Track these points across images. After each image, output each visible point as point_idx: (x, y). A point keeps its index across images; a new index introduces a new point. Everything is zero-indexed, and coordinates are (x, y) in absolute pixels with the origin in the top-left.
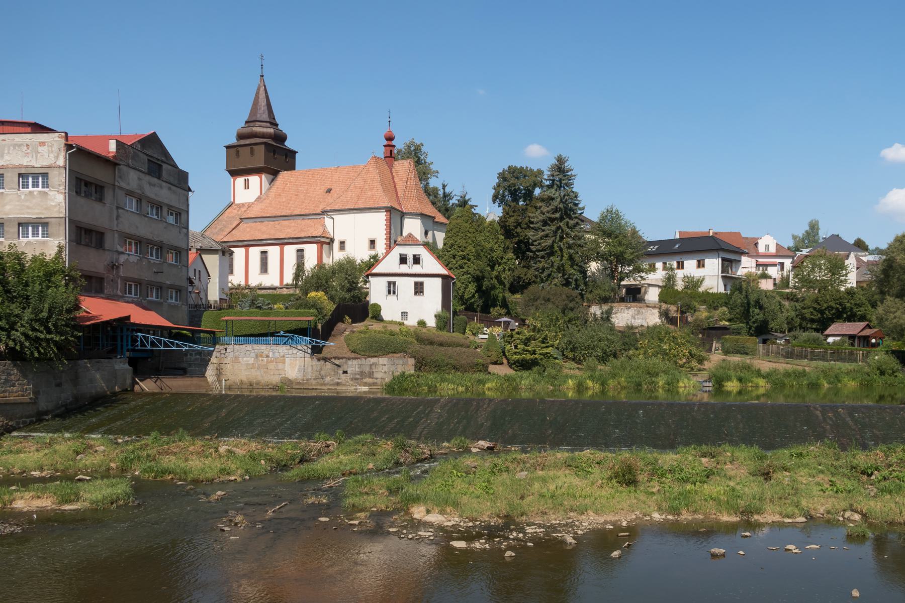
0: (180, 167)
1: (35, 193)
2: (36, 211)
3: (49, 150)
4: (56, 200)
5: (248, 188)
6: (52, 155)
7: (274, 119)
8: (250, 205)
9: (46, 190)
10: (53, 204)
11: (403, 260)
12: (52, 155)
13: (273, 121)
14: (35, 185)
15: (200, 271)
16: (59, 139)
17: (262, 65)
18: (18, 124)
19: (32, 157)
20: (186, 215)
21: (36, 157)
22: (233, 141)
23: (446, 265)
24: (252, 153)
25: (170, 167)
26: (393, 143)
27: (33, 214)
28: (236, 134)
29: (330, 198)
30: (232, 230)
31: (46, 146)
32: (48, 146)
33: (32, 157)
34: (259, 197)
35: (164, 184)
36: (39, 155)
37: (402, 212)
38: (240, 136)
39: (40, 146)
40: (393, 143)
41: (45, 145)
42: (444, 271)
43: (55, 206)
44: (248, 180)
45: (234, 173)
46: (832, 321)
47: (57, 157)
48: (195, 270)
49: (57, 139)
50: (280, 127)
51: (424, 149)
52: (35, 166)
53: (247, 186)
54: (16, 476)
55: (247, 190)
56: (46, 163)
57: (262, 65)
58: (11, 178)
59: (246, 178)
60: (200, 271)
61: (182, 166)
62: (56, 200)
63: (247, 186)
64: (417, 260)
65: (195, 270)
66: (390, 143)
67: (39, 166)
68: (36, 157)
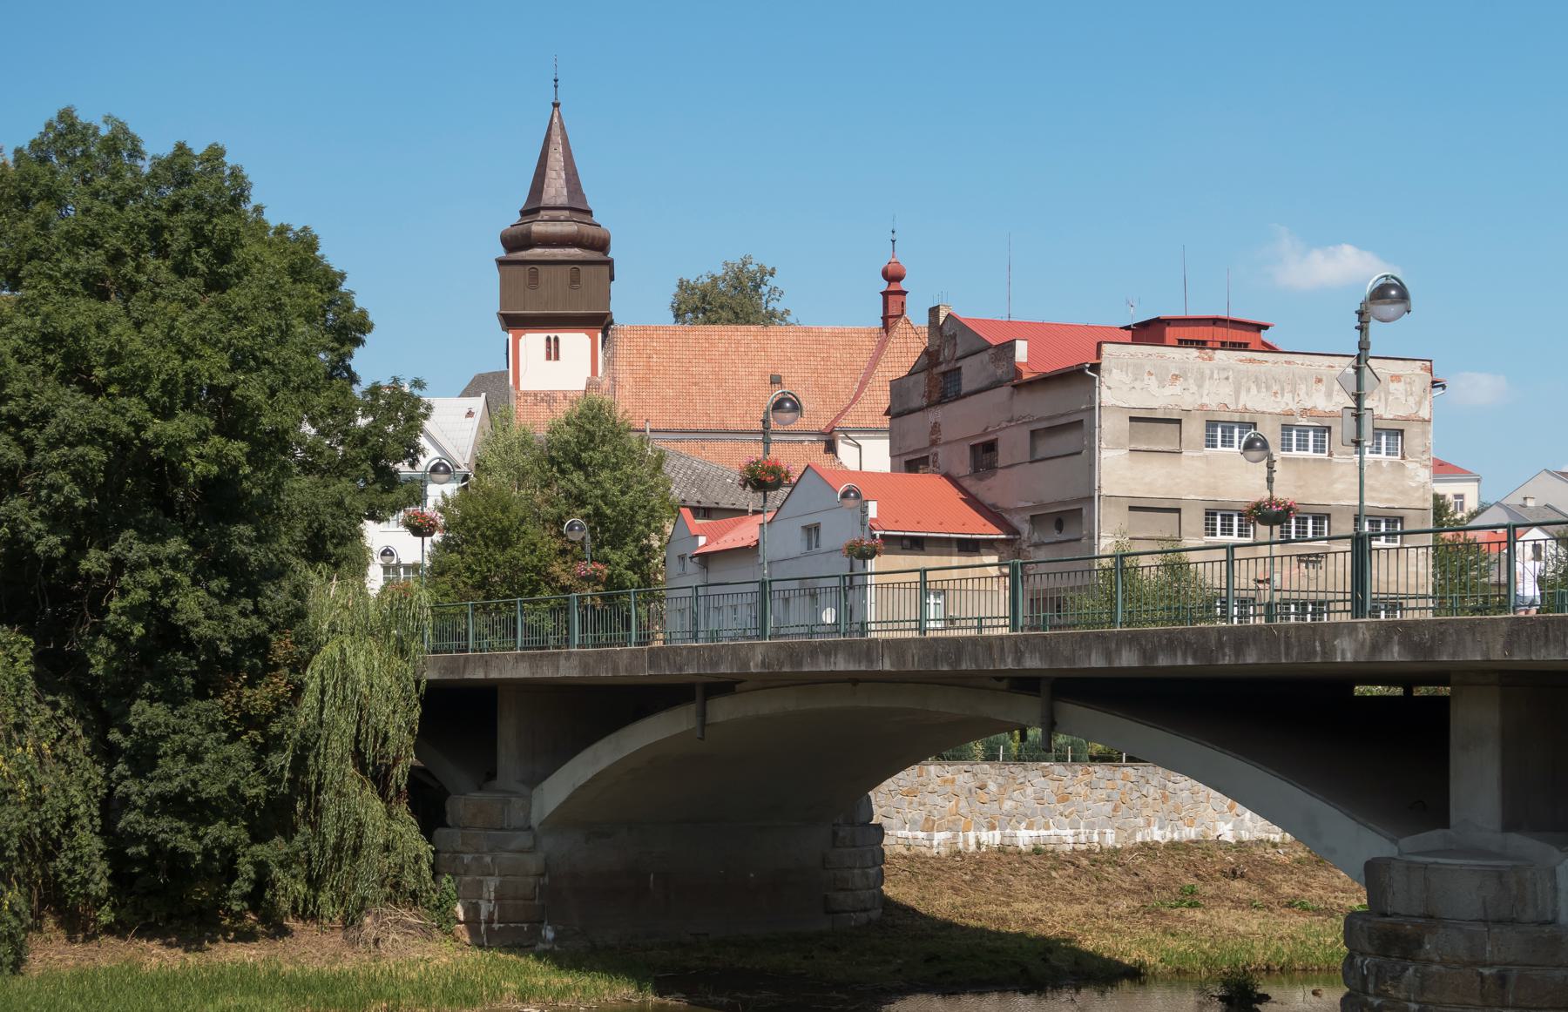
1: (1384, 465)
2: (1386, 496)
3: (1406, 391)
4: (1418, 479)
5: (557, 358)
6: (1411, 399)
9: (1403, 461)
10: (1414, 485)
12: (1411, 400)
14: (1303, 446)
16: (1422, 372)
17: (556, 81)
18: (1192, 322)
19: (1380, 400)
21: (1386, 400)
24: (575, 280)
26: (903, 285)
27: (1380, 502)
31: (1402, 383)
32: (1405, 383)
33: (1380, 400)
36: (1391, 398)
39: (1392, 381)
40: (903, 285)
41: (1400, 381)
43: (1417, 489)
44: (556, 339)
45: (514, 322)
46: (873, 553)
47: (1419, 404)
49: (1418, 371)
50: (596, 218)
52: (1384, 417)
55: (552, 363)
56: (1402, 413)
57: (556, 81)
58: (1194, 430)
59: (552, 336)
62: (1418, 479)
66: (894, 287)
67: (1391, 417)
68: (1386, 400)
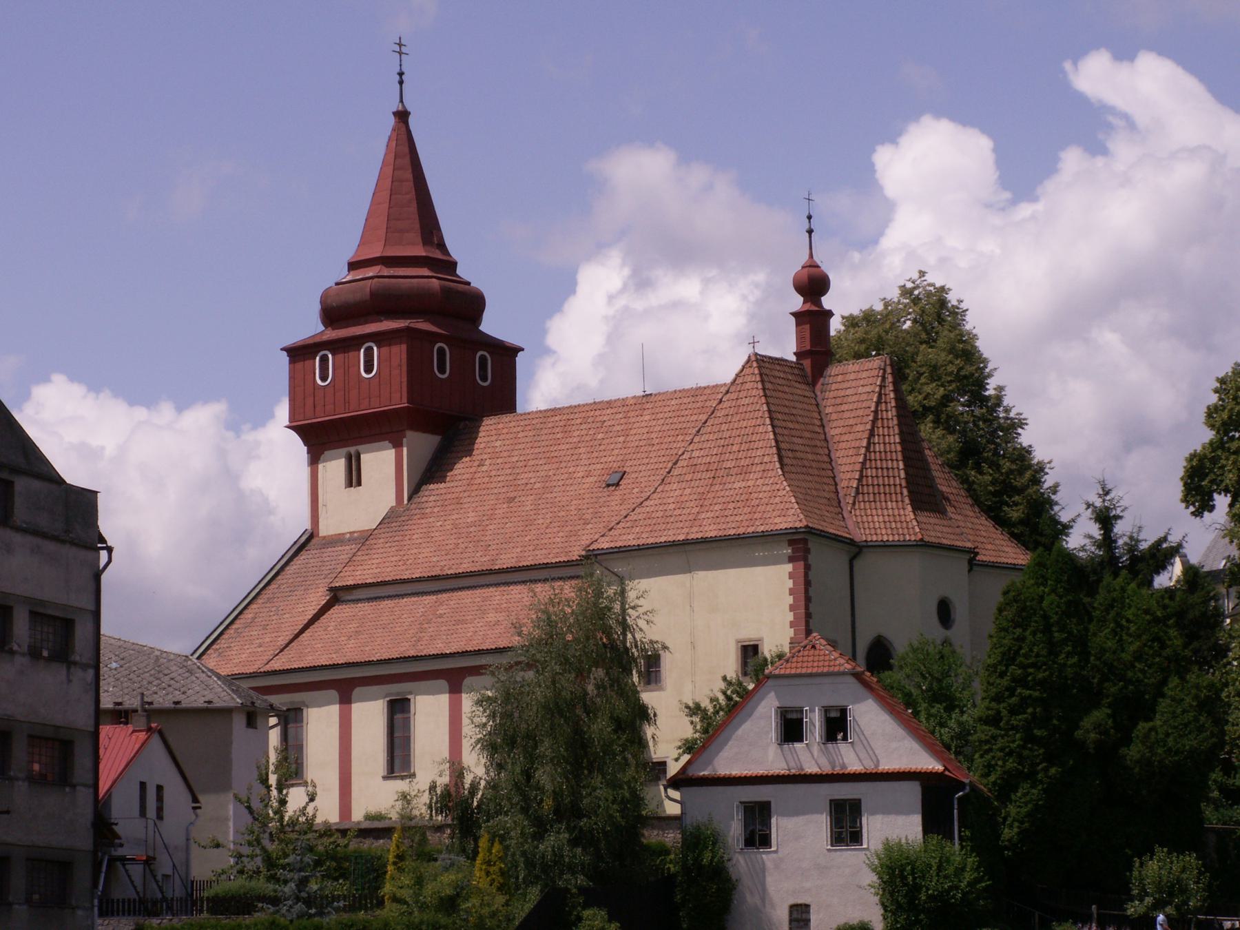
0: (70, 479)
5: (359, 484)
7: (442, 246)
8: (364, 539)
11: (791, 730)
13: (438, 255)
15: (160, 788)
20: (90, 626)
22: (310, 326)
23: (927, 740)
25: (36, 484)
28: (317, 307)
29: (615, 503)
30: (297, 636)
34: (392, 510)
35: (17, 538)
37: (852, 542)
38: (333, 314)
42: (931, 764)
48: (143, 785)
51: (952, 298)
53: (354, 478)
54: (1135, 873)
60: (160, 788)
61: (73, 473)
63: (354, 478)
64: (837, 726)
65: (143, 785)
